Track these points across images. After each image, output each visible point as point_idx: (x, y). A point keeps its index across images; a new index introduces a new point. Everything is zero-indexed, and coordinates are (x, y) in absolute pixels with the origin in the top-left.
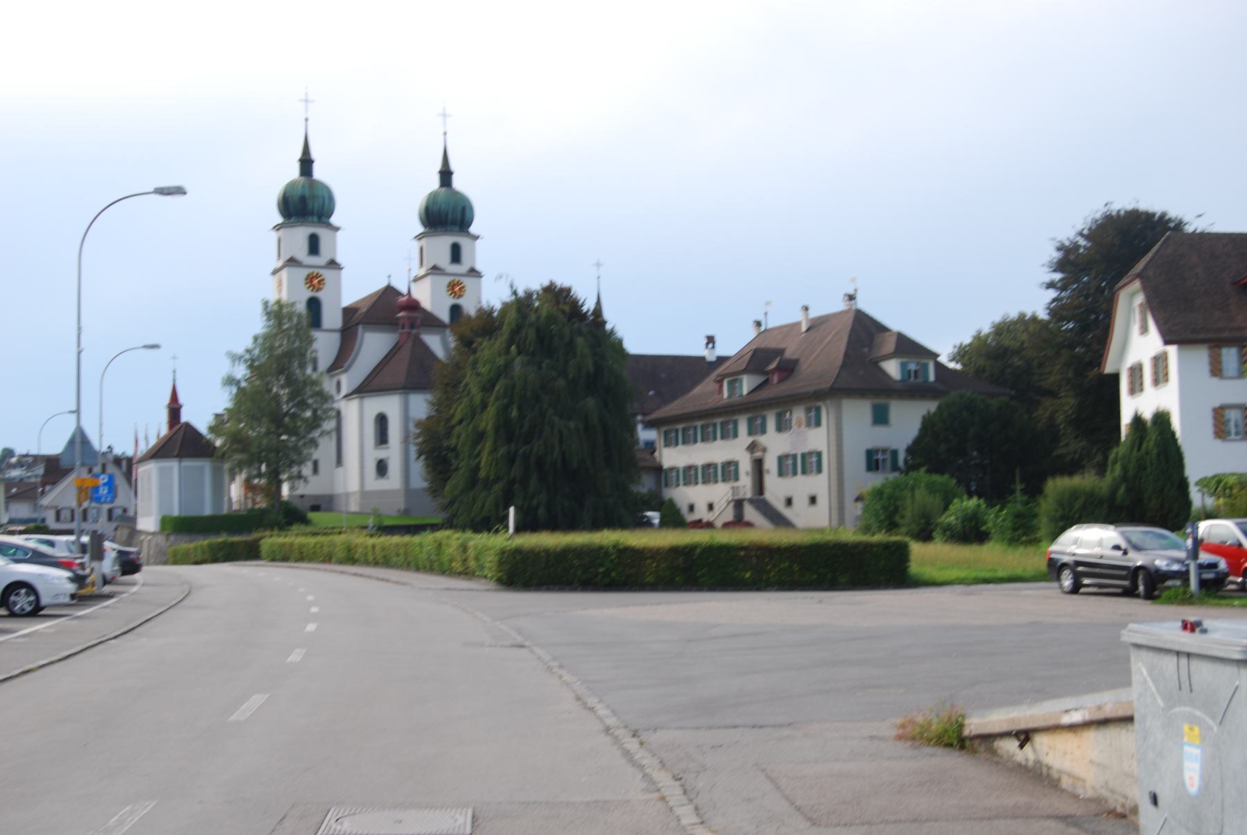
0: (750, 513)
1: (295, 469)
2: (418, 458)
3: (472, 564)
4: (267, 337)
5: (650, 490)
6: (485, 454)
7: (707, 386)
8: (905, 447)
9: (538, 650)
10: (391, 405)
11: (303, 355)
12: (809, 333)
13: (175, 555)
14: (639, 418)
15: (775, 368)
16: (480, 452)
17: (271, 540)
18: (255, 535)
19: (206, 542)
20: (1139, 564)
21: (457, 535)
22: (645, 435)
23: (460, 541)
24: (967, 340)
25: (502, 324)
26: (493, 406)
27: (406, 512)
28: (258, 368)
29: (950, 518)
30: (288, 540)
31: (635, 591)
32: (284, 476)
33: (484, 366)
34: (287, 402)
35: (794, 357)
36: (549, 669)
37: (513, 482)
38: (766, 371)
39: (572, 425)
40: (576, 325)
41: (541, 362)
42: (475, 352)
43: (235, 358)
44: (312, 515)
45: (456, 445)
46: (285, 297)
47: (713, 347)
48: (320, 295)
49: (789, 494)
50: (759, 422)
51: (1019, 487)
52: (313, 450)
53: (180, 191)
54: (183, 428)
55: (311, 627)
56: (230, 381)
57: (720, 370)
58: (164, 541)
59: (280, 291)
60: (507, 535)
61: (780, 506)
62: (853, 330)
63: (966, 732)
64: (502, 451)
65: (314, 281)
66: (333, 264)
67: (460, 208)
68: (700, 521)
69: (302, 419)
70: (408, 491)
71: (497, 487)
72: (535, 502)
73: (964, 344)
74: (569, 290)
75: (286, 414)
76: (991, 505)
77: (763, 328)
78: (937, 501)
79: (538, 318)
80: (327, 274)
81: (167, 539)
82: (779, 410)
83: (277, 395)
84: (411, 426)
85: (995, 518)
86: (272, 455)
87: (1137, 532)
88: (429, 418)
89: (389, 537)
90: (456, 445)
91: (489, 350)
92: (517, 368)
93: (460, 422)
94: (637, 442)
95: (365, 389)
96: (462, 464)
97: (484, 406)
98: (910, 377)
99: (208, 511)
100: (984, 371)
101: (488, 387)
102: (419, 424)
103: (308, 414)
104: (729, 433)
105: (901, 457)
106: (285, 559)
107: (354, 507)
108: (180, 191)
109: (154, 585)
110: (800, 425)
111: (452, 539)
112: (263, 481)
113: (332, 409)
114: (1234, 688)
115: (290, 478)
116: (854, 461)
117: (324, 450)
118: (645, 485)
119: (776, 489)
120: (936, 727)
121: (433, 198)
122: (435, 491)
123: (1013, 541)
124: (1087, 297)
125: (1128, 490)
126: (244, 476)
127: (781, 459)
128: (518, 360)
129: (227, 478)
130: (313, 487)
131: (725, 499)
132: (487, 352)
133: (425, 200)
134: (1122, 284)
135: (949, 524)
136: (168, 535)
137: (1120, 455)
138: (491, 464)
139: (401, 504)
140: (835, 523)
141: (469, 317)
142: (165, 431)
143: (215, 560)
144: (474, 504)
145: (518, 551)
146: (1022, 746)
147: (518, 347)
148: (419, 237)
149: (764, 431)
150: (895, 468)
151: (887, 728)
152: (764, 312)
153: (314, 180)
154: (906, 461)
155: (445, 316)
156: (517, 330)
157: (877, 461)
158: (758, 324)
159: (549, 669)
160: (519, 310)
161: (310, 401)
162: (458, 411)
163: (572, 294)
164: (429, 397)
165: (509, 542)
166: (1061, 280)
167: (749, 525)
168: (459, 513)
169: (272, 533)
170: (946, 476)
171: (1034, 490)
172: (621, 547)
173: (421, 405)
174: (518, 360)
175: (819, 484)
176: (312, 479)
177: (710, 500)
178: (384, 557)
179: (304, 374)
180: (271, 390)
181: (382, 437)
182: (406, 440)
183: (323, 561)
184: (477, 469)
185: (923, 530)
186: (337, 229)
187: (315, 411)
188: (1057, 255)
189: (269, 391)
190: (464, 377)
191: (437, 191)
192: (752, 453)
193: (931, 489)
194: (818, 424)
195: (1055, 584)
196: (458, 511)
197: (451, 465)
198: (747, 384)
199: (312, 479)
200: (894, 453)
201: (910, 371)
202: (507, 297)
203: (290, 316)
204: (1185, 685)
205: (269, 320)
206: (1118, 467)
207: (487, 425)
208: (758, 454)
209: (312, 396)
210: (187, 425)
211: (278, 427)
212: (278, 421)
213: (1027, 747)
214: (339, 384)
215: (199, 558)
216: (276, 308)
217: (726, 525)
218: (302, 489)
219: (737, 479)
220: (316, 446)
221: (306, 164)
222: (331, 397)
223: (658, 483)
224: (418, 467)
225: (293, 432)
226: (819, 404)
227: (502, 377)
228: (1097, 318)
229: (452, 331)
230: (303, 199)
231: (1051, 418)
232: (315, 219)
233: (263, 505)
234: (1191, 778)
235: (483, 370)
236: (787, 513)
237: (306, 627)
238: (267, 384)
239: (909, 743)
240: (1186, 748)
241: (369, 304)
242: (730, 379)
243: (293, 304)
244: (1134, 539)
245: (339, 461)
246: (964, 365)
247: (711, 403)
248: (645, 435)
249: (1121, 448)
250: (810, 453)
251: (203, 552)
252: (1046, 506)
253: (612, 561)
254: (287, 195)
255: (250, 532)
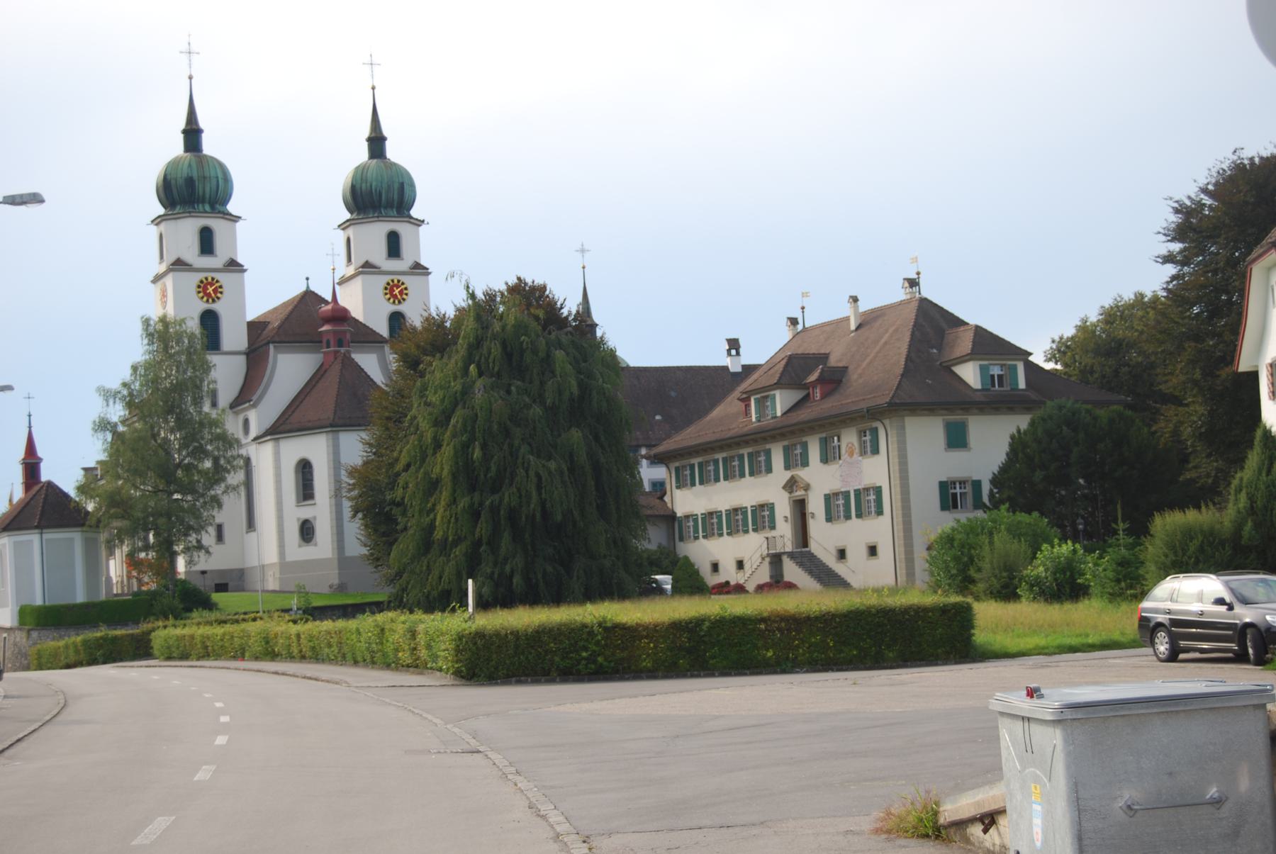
0: (792, 572)
1: (193, 538)
2: (354, 516)
3: (423, 653)
4: (148, 366)
5: (659, 546)
6: (440, 509)
7: (728, 407)
8: (990, 476)
9: (492, 755)
10: (315, 448)
11: (199, 388)
12: (859, 332)
13: (39, 656)
14: (643, 451)
15: (817, 380)
16: (434, 505)
17: (165, 633)
18: (145, 627)
19: (79, 639)
20: (1248, 620)
21: (403, 618)
22: (649, 473)
23: (406, 626)
24: (1069, 332)
25: (457, 337)
26: (448, 445)
27: (341, 588)
28: (137, 406)
29: (1038, 569)
30: (187, 631)
31: (628, 679)
32: (179, 548)
33: (435, 393)
34: (179, 451)
35: (841, 365)
36: (505, 776)
37: (478, 543)
38: (805, 384)
39: (552, 465)
40: (553, 336)
41: (510, 385)
42: (422, 375)
43: (108, 395)
44: (216, 597)
45: (403, 498)
46: (170, 311)
47: (738, 354)
48: (216, 307)
49: (840, 545)
50: (798, 451)
51: (1121, 526)
52: (215, 513)
53: (36, 199)
54: (43, 492)
55: (221, 740)
56: (103, 425)
57: (745, 386)
58: (24, 640)
59: (164, 304)
60: (466, 615)
61: (830, 560)
62: (916, 325)
63: (942, 821)
64: (463, 502)
65: (209, 289)
66: (234, 266)
67: (396, 186)
68: (727, 583)
69: (199, 472)
70: (343, 561)
71: (458, 551)
72: (508, 568)
73: (1065, 337)
74: (543, 288)
75: (179, 465)
76: (1089, 550)
77: (800, 327)
78: (1023, 547)
79: (503, 328)
80: (224, 279)
81: (29, 636)
82: (824, 435)
83: (166, 440)
84: (345, 478)
85: (1095, 567)
86: (162, 521)
87: (1248, 581)
88: (366, 463)
89: (318, 623)
90: (403, 498)
91: (441, 371)
92: (479, 395)
93: (408, 466)
94: (640, 483)
95: (280, 429)
96: (412, 522)
97: (437, 445)
98: (993, 385)
99: (80, 597)
100: (1092, 372)
101: (441, 421)
102: (352, 472)
103: (208, 464)
104: (760, 467)
105: (986, 488)
106: (184, 656)
107: (272, 584)
108: (36, 199)
109: (19, 697)
110: (851, 454)
111: (397, 622)
112: (152, 555)
113: (239, 456)
114: (1053, 746)
115: (187, 550)
116: (926, 497)
117: (230, 511)
118: (652, 540)
119: (824, 537)
120: (912, 819)
121: (360, 172)
122: (378, 559)
123: (1115, 597)
124: (1215, 272)
125: (1257, 526)
126: (126, 549)
127: (828, 499)
128: (479, 383)
129: (104, 553)
130: (218, 559)
131: (758, 555)
132: (438, 375)
133: (351, 176)
134: (1256, 255)
135: (1038, 577)
136: (29, 631)
137: (1245, 480)
138: (449, 522)
139: (333, 576)
140: (902, 579)
141: (414, 329)
142: (19, 494)
143: (92, 662)
144: (428, 575)
145: (480, 635)
146: (985, 831)
147: (479, 366)
148: (344, 226)
149: (805, 463)
150: (978, 504)
151: (866, 823)
152: (801, 306)
153: (205, 156)
154: (991, 495)
155: (383, 329)
156: (476, 345)
157: (954, 495)
158: (794, 321)
159: (505, 776)
160: (478, 318)
161: (209, 447)
162: (403, 454)
163: (547, 292)
164: (364, 435)
165: (469, 623)
166: (1181, 252)
167: (791, 586)
168: (410, 587)
169: (167, 623)
170: (1035, 514)
171: (1140, 530)
172: (609, 625)
173: (354, 447)
174: (479, 383)
175: (879, 529)
176: (215, 548)
177: (739, 556)
178: (313, 648)
179: (200, 412)
180: (159, 434)
181: (306, 491)
182: (337, 494)
183: (234, 658)
184: (431, 527)
185: (1005, 586)
186: (235, 219)
187: (216, 460)
188: (1174, 219)
189: (155, 436)
190: (410, 409)
191: (367, 162)
192: (790, 493)
193: (1015, 532)
194: (876, 451)
195: (1149, 650)
196: (408, 583)
197: (397, 524)
198: (781, 401)
199: (215, 548)
200: (977, 485)
201: (993, 376)
202: (462, 300)
203: (179, 337)
204: (1029, 749)
205: (151, 343)
206: (1243, 497)
207: (442, 469)
208: (799, 493)
209: (211, 441)
210: (50, 485)
211: (168, 483)
212: (167, 475)
213: (992, 831)
214: (246, 422)
215: (72, 658)
216: (160, 327)
217: (760, 588)
218: (203, 563)
219: (773, 527)
220: (220, 506)
221: (192, 135)
222: (238, 441)
223: (671, 537)
224: (354, 529)
225: (188, 489)
226: (878, 424)
227: (460, 406)
228: (1230, 300)
229: (392, 348)
230: (190, 181)
231: (1176, 433)
232: (207, 208)
233: (153, 586)
234: (1037, 833)
235: (434, 398)
236: (839, 568)
237: (215, 740)
238: (152, 428)
239: (884, 836)
240: (1034, 805)
241: (283, 316)
242: (758, 396)
243: (183, 321)
244: (1247, 593)
245: (251, 524)
246: (1066, 365)
247: (738, 427)
248: (649, 473)
249: (1246, 471)
250: (867, 490)
251: (77, 651)
252: (1153, 549)
253: (598, 643)
254: (169, 177)
255: (137, 622)
